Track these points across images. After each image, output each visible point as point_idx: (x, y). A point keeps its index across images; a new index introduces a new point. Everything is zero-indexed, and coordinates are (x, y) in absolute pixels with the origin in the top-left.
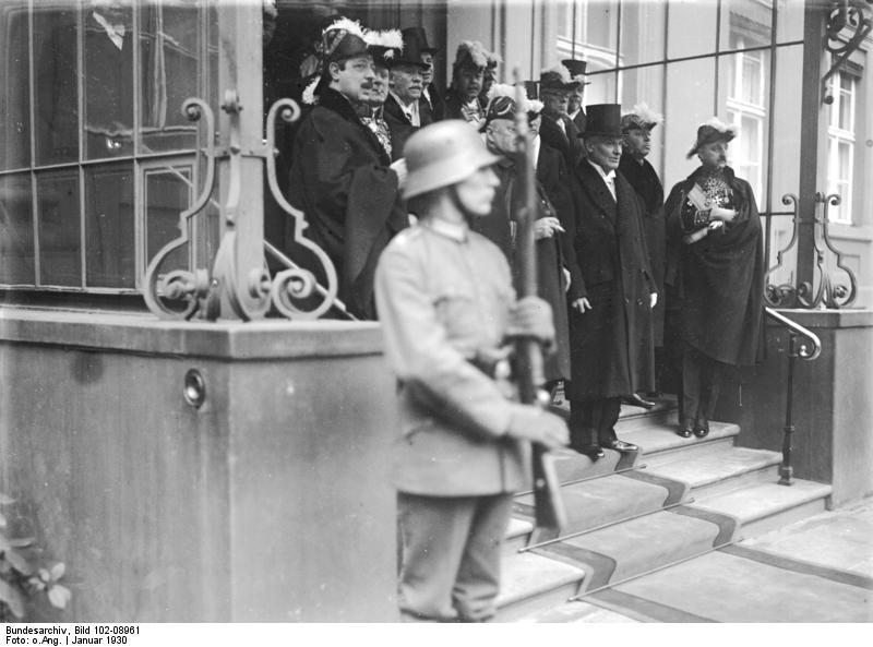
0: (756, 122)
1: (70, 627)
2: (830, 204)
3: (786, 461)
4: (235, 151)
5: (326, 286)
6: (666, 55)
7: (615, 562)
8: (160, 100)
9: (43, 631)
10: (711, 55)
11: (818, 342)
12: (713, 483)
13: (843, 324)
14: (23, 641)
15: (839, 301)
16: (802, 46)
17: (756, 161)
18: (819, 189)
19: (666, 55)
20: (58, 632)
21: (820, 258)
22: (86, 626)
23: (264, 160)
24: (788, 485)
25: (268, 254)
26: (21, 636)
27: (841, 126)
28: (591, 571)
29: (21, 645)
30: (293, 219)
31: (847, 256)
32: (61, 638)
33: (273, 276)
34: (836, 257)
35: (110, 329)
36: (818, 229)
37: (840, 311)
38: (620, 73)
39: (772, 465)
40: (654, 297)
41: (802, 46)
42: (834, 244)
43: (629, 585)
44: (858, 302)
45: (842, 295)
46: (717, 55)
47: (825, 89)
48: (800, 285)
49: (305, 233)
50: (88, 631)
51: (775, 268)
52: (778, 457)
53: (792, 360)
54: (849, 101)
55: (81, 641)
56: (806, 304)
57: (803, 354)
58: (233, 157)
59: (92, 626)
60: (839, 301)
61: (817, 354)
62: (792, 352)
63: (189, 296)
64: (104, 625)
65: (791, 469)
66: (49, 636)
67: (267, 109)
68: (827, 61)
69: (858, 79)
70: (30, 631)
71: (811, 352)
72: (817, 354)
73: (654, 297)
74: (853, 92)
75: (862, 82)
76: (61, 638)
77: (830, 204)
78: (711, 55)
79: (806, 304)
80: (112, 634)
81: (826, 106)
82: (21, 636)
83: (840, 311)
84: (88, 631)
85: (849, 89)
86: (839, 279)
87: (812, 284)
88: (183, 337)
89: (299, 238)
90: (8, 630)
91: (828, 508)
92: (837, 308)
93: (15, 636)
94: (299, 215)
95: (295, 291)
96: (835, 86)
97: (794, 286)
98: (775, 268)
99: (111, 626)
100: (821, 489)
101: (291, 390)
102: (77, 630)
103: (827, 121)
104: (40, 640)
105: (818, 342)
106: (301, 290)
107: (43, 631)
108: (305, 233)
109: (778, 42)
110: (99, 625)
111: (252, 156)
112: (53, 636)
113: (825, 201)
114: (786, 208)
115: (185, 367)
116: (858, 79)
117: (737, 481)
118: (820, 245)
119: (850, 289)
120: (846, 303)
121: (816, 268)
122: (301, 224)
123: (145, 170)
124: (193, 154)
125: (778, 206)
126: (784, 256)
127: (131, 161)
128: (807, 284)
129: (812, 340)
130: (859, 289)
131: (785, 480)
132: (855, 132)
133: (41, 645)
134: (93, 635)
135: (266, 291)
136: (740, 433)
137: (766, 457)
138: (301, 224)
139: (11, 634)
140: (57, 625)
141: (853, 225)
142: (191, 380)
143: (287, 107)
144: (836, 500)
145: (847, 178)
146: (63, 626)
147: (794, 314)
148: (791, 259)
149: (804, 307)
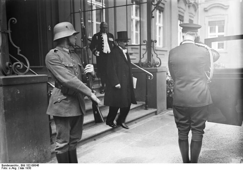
1: (20, 164)
2: (154, 42)
3: (146, 104)
5: (27, 66)
9: (12, 166)
11: (152, 75)
12: (147, 115)
13: (158, 71)
14: (6, 168)
15: (157, 66)
16: (146, 4)
18: (152, 39)
20: (16, 166)
21: (153, 56)
22: (24, 164)
23: (8, 34)
24: (147, 109)
25: (10, 57)
26: (6, 167)
27: (159, 23)
30: (17, 49)
32: (17, 167)
33: (13, 64)
34: (156, 55)
35: (233, 160)
36: (152, 49)
37: (157, 68)
40: (105, 85)
41: (146, 4)
42: (156, 52)
44: (162, 66)
45: (158, 64)
46: (127, 5)
47: (152, 14)
48: (148, 62)
49: (20, 53)
53: (147, 80)
54: (161, 16)
56: (150, 67)
57: (149, 78)
59: (26, 164)
60: (157, 66)
61: (152, 78)
62: (147, 78)
64: (29, 164)
65: (147, 106)
66: (14, 167)
68: (153, 7)
69: (163, 11)
70: (8, 165)
71: (151, 78)
72: (152, 78)
73: (105, 85)
75: (164, 12)
76: (17, 167)
77: (154, 42)
79: (150, 67)
81: (153, 19)
82: (6, 167)
83: (157, 68)
84: (24, 166)
85: (161, 13)
86: (157, 60)
87: (151, 62)
89: (18, 54)
90: (2, 165)
91: (156, 114)
92: (157, 67)
93: (4, 167)
94: (18, 48)
95: (18, 67)
96: (157, 13)
97: (147, 62)
98: (142, 58)
99: (31, 164)
100: (154, 110)
102: (21, 165)
103: (132, 14)
105: (152, 75)
106: (20, 67)
107: (12, 166)
108: (20, 53)
110: (27, 164)
112: (15, 167)
113: (153, 42)
114: (144, 44)
116: (163, 11)
117: (135, 109)
118: (153, 52)
119: (160, 62)
120: (159, 66)
121: (152, 58)
126: (144, 55)
128: (150, 62)
129: (151, 75)
130: (162, 62)
135: (11, 68)
137: (141, 103)
138: (19, 50)
139: (3, 167)
140: (16, 164)
141: (163, 47)
144: (158, 113)
146: (18, 164)
147: (148, 69)
148: (146, 56)
149: (149, 67)
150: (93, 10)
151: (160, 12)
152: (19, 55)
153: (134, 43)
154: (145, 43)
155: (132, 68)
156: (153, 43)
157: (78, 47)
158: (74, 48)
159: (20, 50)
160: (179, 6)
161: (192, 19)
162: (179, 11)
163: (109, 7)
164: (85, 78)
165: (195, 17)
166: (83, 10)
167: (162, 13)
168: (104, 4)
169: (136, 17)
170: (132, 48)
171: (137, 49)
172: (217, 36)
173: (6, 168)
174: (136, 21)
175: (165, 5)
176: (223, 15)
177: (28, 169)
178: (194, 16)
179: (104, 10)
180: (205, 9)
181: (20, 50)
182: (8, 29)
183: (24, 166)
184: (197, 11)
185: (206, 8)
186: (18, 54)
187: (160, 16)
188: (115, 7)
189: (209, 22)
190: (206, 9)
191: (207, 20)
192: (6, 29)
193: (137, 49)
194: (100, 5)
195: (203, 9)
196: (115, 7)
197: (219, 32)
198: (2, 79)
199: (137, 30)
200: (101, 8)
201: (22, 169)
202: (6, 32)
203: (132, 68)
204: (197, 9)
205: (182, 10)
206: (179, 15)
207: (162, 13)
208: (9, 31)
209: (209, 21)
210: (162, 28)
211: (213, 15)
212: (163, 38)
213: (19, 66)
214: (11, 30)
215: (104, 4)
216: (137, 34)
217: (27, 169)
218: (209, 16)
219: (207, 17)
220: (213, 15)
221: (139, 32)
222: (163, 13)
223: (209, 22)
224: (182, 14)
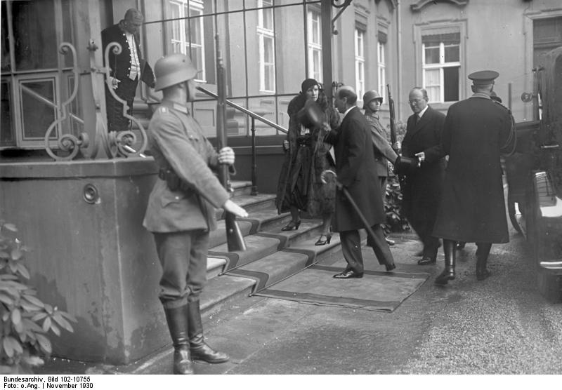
1: (45, 377)
4: (93, 70)
6: (244, 14)
7: (268, 275)
8: (360, 79)
9: (27, 380)
10: (252, 97)
14: (15, 386)
17: (200, 44)
19: (244, 14)
20: (38, 380)
22: (55, 376)
26: (13, 383)
27: (314, 41)
28: (259, 280)
32: (39, 384)
43: (275, 286)
49: (129, 112)
51: (277, 132)
52: (250, 183)
58: (92, 74)
59: (60, 376)
63: (225, 166)
66: (31, 383)
70: (20, 380)
76: (39, 384)
78: (252, 97)
80: (83, 382)
82: (13, 383)
84: (56, 380)
85: (316, 20)
88: (81, 168)
90: (5, 379)
93: (10, 383)
101: (138, 191)
102: (50, 379)
104: (26, 386)
107: (27, 380)
110: (63, 376)
111: (99, 73)
112: (34, 383)
115: (83, 183)
122: (126, 108)
123: (19, 81)
124: (57, 71)
127: (10, 75)
131: (253, 194)
134: (72, 383)
138: (126, 108)
139: (7, 382)
140: (37, 376)
141: (207, 83)
142: (88, 189)
143: (113, 47)
146: (40, 376)
150: (185, 18)
152: (125, 118)
153: (263, 90)
155: (541, 118)
157: (155, 101)
158: (146, 103)
159: (128, 108)
160: (379, 15)
161: (385, 31)
162: (379, 25)
163: (230, 11)
164: (216, 167)
165: (390, 26)
167: (362, 35)
169: (265, 29)
170: (262, 102)
171: (270, 103)
173: (15, 386)
174: (265, 38)
175: (369, 19)
176: (457, 21)
178: (389, 23)
180: (412, 6)
181: (128, 108)
182: (104, 66)
183: (56, 380)
184: (395, 10)
185: (415, 6)
186: (125, 114)
187: (359, 40)
188: (163, 21)
189: (423, 38)
190: (414, 8)
191: (419, 33)
192: (102, 65)
193: (270, 103)
195: (409, 6)
197: (446, 61)
198: (116, 163)
199: (266, 60)
201: (51, 389)
202: (102, 71)
203: (541, 118)
204: (395, 6)
205: (362, 11)
206: (357, 22)
207: (362, 35)
209: (424, 34)
211: (432, 22)
213: (130, 139)
214: (111, 66)
216: (267, 69)
218: (423, 24)
219: (417, 25)
220: (432, 22)
221: (272, 64)
222: (364, 35)
223: (423, 38)
224: (363, 21)
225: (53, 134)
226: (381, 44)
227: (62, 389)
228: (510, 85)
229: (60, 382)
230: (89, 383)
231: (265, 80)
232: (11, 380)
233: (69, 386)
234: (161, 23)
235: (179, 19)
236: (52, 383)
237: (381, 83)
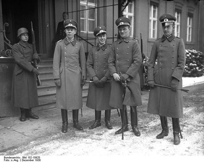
0: (85, 6)
6: (104, 6)
14: (9, 160)
20: (18, 158)
26: (8, 159)
29: (8, 161)
31: (95, 41)
32: (19, 160)
38: (88, 10)
39: (24, 135)
50: (26, 158)
55: (24, 160)
66: (15, 159)
67: (3, 25)
69: (181, 13)
70: (10, 158)
74: (157, 10)
76: (19, 160)
82: (8, 159)
84: (26, 158)
85: (156, 8)
90: (5, 157)
93: (7, 159)
102: (23, 157)
107: (14, 158)
109: (114, 4)
112: (17, 159)
116: (181, 13)
125: (115, 37)
132: (134, 13)
133: (13, 161)
136: (186, 41)
143: (7, 24)
145: (85, 18)
151: (178, 14)
154: (117, 37)
156: (189, 39)
163: (100, 6)
166: (75, 10)
168: (96, 4)
172: (150, 18)
173: (9, 160)
177: (38, 161)
179: (96, 9)
181: (10, 42)
187: (154, 11)
188: (113, 5)
194: (93, 5)
196: (113, 5)
200: (94, 7)
208: (4, 31)
210: (191, 29)
212: (157, 31)
215: (96, 4)
217: (36, 161)
225: (13, 57)
226: (190, 17)
227: (28, 161)
228: (141, 34)
229: (27, 159)
230: (39, 159)
231: (153, 35)
232: (7, 158)
233: (30, 160)
234: (76, 12)
235: (84, 10)
236: (24, 159)
237: (154, 28)
